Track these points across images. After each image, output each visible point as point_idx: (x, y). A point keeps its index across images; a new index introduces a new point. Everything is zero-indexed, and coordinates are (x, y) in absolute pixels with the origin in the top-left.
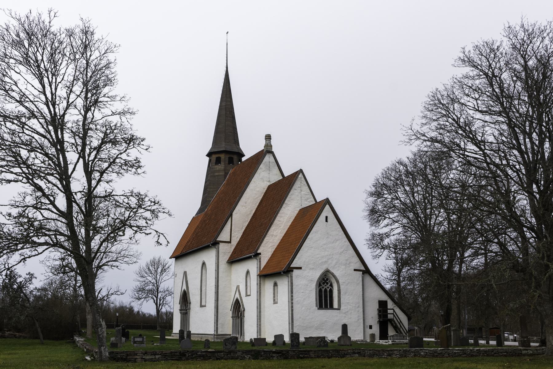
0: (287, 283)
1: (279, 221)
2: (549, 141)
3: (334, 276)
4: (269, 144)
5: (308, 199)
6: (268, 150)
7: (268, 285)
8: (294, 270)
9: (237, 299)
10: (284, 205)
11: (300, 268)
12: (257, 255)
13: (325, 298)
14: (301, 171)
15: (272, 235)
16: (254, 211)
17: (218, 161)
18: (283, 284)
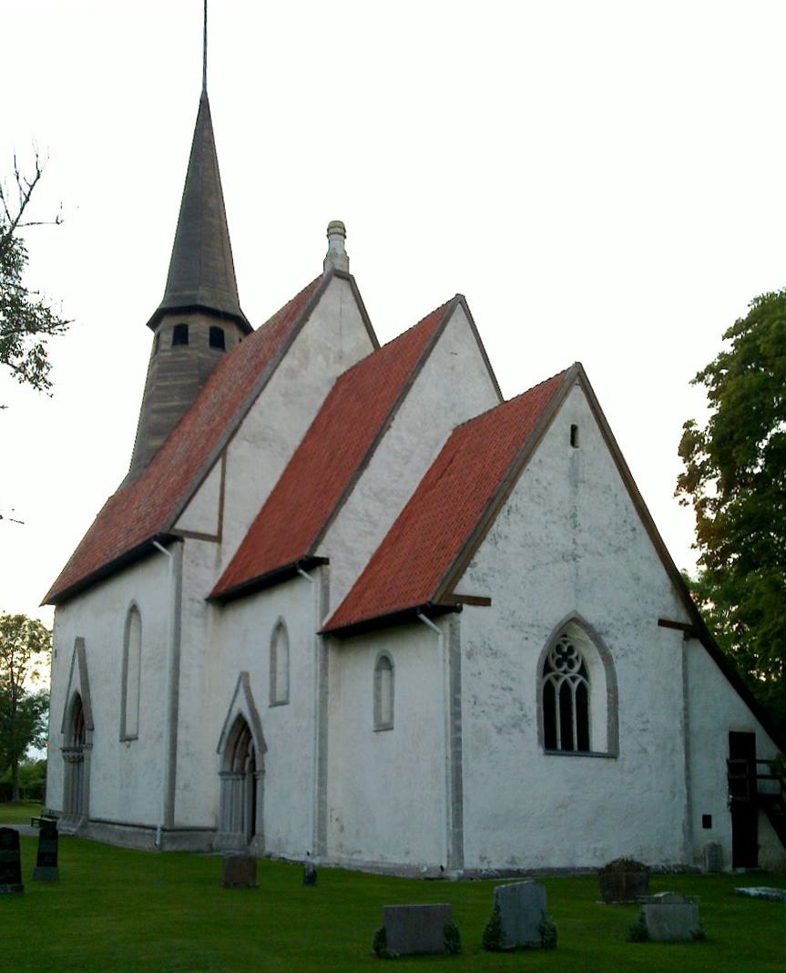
2: (750, 499)
4: (340, 252)
6: (338, 272)
7: (360, 665)
9: (240, 718)
11: (485, 602)
14: (460, 300)
17: (181, 336)
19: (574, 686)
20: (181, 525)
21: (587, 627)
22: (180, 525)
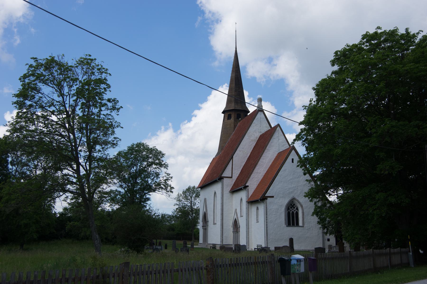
0: (263, 207)
1: (262, 162)
3: (299, 202)
5: (284, 145)
7: (253, 209)
8: (268, 198)
9: (235, 219)
10: (266, 151)
11: (273, 197)
12: (246, 187)
13: (292, 219)
15: (257, 173)
16: (249, 155)
18: (262, 207)
19: (295, 212)
20: (223, 175)
22: (223, 175)
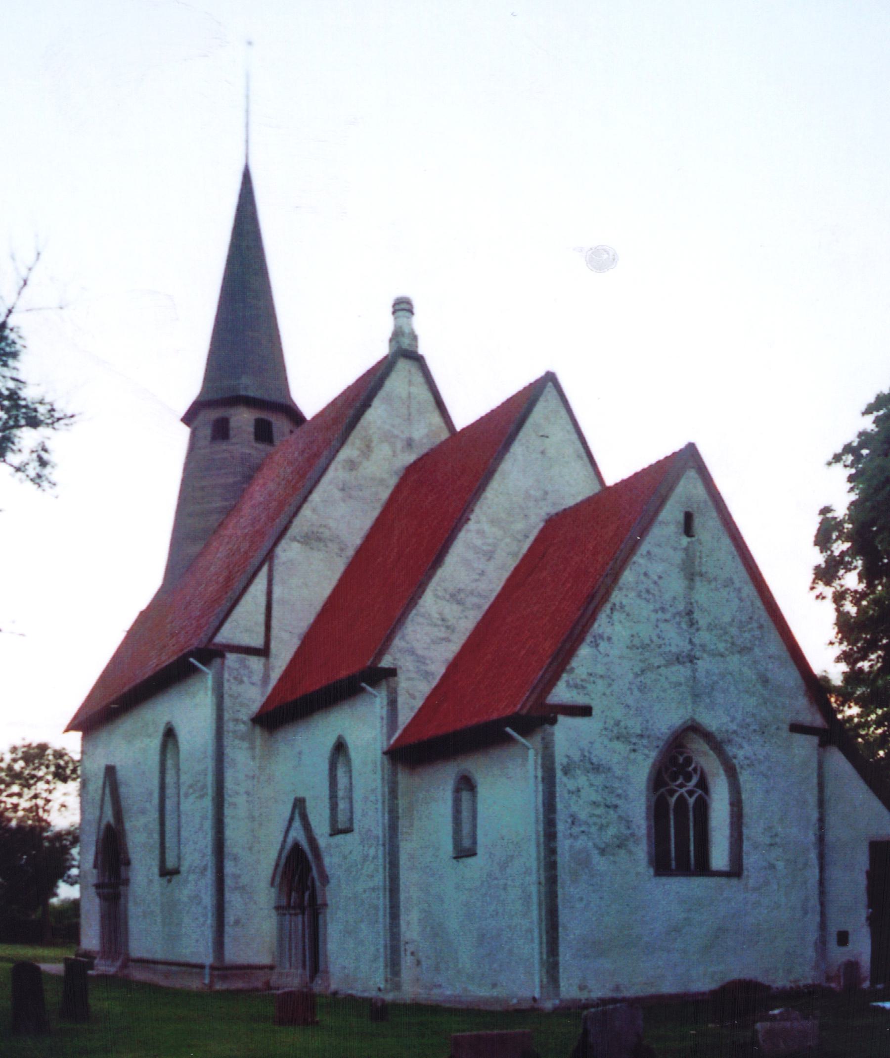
8: (561, 719)
14: (550, 379)
17: (221, 431)
21: (707, 736)
